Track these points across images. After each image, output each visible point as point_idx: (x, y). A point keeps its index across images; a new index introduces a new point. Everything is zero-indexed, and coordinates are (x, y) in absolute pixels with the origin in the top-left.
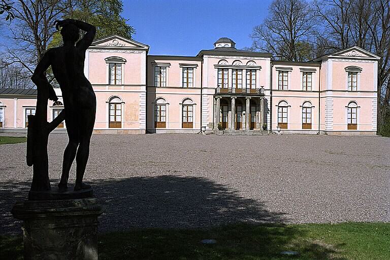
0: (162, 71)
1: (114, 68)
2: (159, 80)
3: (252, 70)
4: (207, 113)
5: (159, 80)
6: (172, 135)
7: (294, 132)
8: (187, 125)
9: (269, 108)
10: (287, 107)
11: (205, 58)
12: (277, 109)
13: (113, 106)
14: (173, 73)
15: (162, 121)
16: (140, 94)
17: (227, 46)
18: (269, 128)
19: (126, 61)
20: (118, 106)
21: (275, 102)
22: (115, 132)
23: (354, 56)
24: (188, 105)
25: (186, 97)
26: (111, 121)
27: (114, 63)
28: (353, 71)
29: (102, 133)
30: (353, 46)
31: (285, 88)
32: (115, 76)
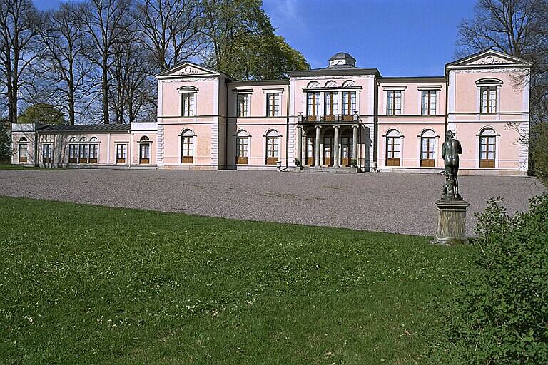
0: (245, 98)
1: (427, 95)
2: (241, 110)
3: (350, 92)
4: (290, 146)
5: (241, 110)
6: (255, 173)
7: (409, 171)
8: (270, 160)
9: (372, 139)
10: (495, 136)
11: (452, 74)
12: (420, 140)
13: (425, 142)
14: (256, 99)
15: (430, 158)
16: (212, 126)
17: (340, 64)
18: (372, 165)
19: (198, 90)
20: (491, 140)
21: (382, 131)
22: (187, 168)
23: (490, 64)
24: (273, 138)
25: (484, 125)
26: (482, 158)
27: (187, 93)
28: (488, 86)
29: (174, 168)
30: (488, 50)
31: (432, 113)
32: (273, 107)
